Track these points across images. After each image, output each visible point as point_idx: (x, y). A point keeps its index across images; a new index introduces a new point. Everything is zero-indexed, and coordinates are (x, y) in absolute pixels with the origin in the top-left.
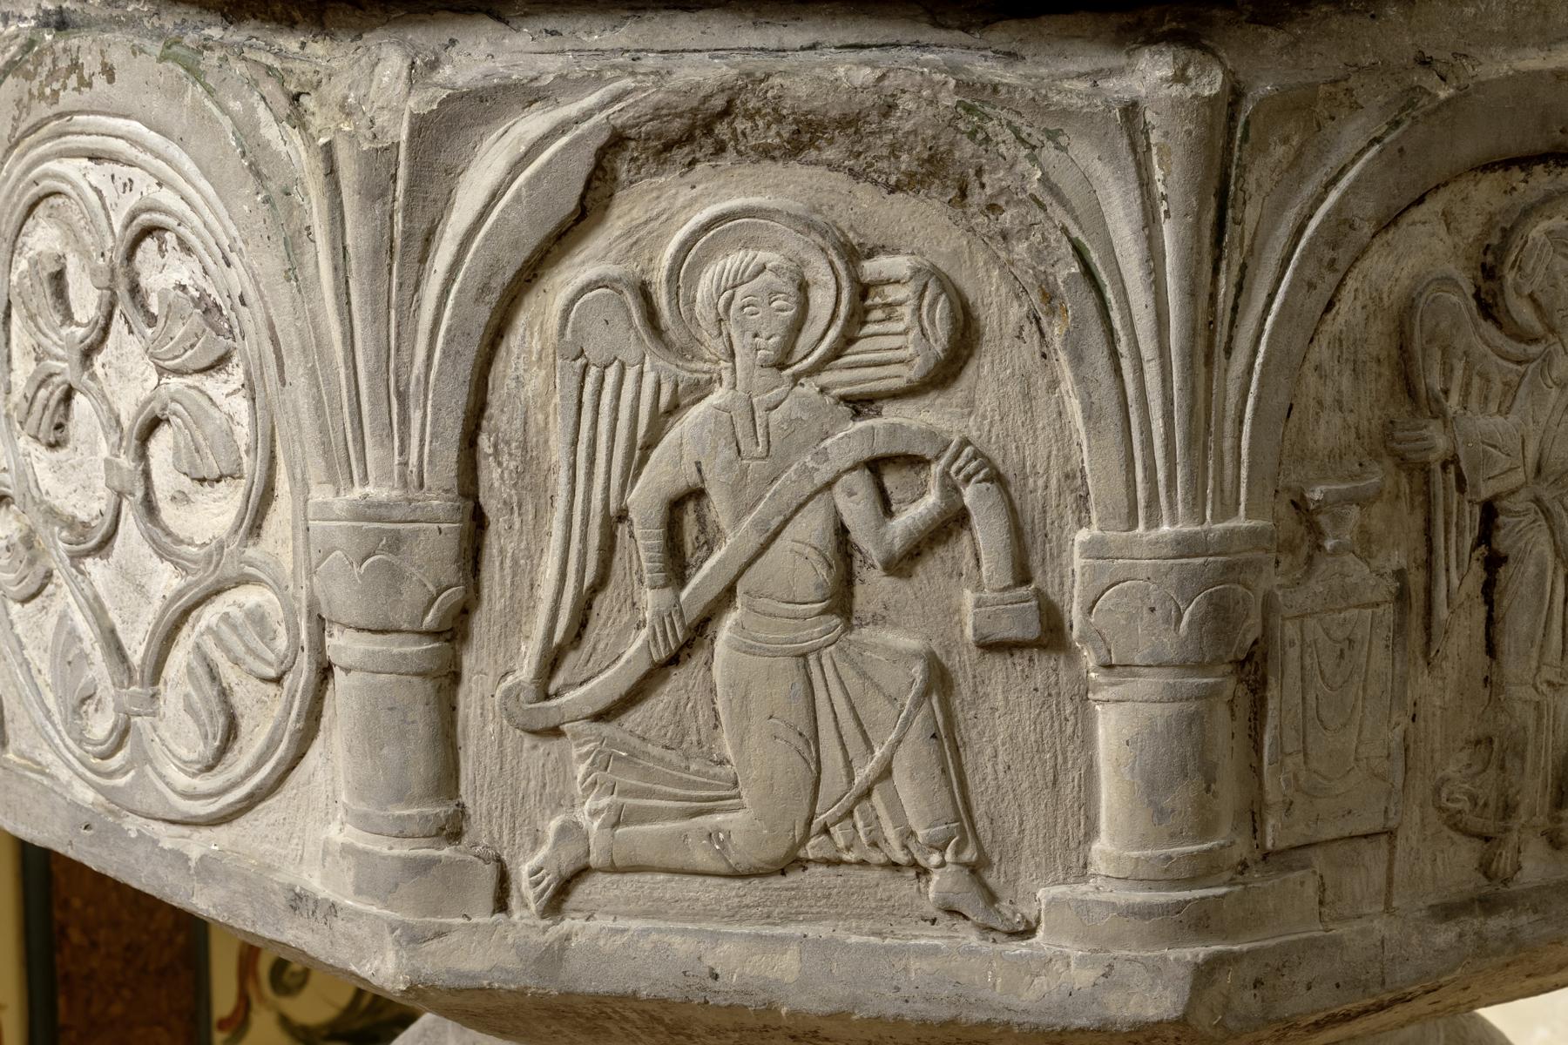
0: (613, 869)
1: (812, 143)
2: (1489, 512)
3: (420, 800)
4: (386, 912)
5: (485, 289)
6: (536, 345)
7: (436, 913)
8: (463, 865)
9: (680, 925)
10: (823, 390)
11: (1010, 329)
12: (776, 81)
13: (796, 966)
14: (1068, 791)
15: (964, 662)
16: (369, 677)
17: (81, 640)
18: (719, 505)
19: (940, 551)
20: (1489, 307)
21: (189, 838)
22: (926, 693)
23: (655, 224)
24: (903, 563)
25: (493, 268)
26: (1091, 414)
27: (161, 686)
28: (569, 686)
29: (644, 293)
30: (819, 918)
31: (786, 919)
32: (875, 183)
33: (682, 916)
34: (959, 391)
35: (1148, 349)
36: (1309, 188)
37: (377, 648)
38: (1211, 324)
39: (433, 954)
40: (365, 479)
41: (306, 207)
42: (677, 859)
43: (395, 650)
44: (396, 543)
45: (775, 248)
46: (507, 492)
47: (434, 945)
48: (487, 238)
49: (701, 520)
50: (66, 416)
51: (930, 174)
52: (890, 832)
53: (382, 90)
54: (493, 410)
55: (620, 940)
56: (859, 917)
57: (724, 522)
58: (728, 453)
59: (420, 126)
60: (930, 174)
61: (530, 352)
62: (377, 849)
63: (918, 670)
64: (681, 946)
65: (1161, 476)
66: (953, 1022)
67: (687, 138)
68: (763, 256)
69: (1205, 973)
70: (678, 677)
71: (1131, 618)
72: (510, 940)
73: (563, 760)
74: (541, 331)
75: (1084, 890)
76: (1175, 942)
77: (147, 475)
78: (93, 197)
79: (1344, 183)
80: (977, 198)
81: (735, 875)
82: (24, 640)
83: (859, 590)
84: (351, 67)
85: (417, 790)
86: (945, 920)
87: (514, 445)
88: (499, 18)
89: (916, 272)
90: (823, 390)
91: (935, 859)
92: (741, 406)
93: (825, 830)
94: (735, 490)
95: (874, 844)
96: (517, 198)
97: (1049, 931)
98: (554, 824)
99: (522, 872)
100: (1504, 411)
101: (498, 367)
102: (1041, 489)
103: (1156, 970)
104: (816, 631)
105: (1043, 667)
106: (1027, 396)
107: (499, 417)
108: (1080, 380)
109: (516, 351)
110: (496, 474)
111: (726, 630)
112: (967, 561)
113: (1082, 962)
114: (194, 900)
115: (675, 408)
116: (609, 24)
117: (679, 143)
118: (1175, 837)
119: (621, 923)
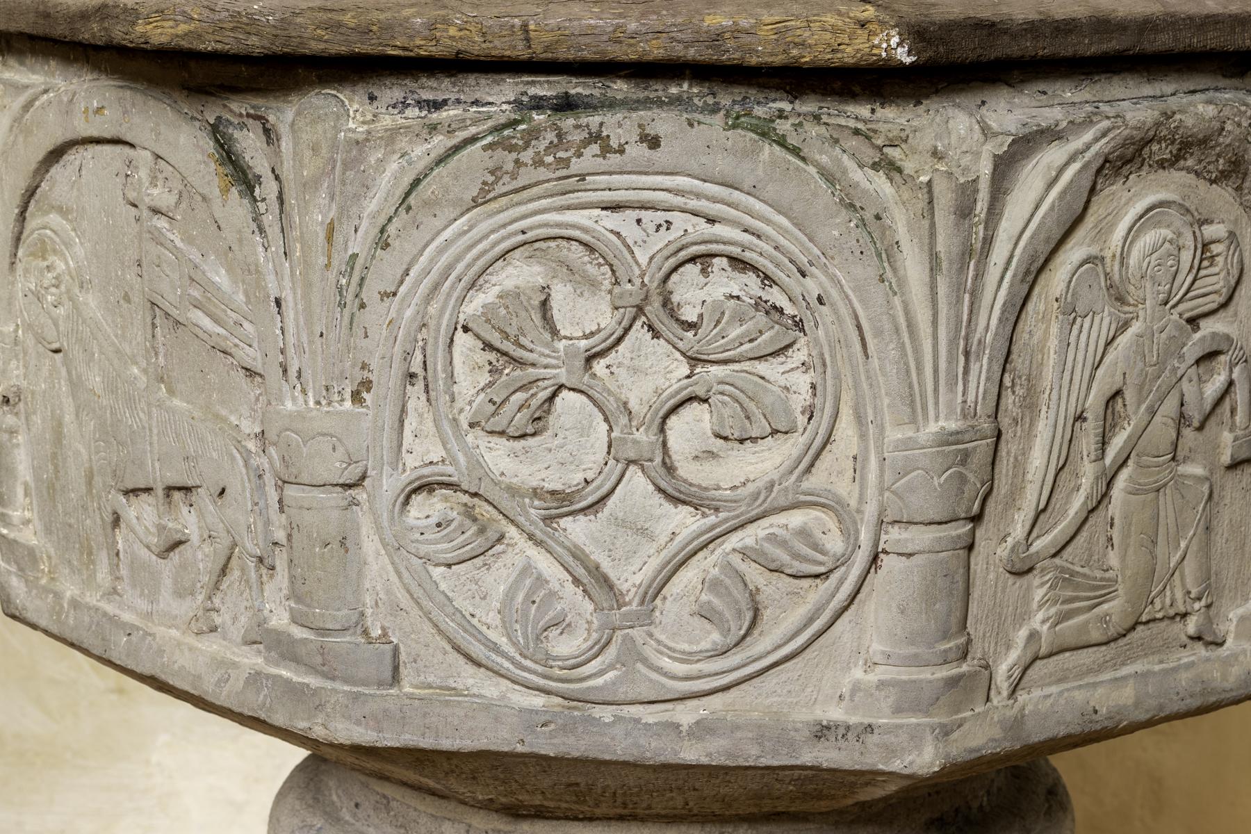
4: (927, 720)
6: (1042, 307)
9: (1076, 684)
10: (1181, 315)
12: (1178, 117)
16: (933, 556)
17: (547, 582)
18: (1129, 395)
21: (673, 710)
23: (1110, 218)
25: (1033, 259)
27: (658, 601)
28: (1038, 537)
32: (1205, 178)
37: (942, 534)
39: (956, 741)
41: (894, 227)
42: (1084, 639)
43: (954, 533)
46: (1016, 411)
48: (1032, 237)
50: (548, 412)
51: (1233, 171)
53: (962, 140)
55: (1050, 701)
56: (1153, 653)
60: (1233, 171)
61: (1038, 313)
62: (922, 676)
63: (1205, 488)
64: (1079, 696)
72: (996, 719)
73: (1029, 588)
74: (1046, 298)
77: (664, 444)
82: (450, 594)
84: (931, 124)
87: (1024, 378)
88: (1010, 85)
93: (1152, 603)
96: (1052, 208)
107: (1018, 361)
109: (1031, 313)
110: (1010, 401)
111: (1124, 475)
114: (682, 755)
116: (1073, 85)
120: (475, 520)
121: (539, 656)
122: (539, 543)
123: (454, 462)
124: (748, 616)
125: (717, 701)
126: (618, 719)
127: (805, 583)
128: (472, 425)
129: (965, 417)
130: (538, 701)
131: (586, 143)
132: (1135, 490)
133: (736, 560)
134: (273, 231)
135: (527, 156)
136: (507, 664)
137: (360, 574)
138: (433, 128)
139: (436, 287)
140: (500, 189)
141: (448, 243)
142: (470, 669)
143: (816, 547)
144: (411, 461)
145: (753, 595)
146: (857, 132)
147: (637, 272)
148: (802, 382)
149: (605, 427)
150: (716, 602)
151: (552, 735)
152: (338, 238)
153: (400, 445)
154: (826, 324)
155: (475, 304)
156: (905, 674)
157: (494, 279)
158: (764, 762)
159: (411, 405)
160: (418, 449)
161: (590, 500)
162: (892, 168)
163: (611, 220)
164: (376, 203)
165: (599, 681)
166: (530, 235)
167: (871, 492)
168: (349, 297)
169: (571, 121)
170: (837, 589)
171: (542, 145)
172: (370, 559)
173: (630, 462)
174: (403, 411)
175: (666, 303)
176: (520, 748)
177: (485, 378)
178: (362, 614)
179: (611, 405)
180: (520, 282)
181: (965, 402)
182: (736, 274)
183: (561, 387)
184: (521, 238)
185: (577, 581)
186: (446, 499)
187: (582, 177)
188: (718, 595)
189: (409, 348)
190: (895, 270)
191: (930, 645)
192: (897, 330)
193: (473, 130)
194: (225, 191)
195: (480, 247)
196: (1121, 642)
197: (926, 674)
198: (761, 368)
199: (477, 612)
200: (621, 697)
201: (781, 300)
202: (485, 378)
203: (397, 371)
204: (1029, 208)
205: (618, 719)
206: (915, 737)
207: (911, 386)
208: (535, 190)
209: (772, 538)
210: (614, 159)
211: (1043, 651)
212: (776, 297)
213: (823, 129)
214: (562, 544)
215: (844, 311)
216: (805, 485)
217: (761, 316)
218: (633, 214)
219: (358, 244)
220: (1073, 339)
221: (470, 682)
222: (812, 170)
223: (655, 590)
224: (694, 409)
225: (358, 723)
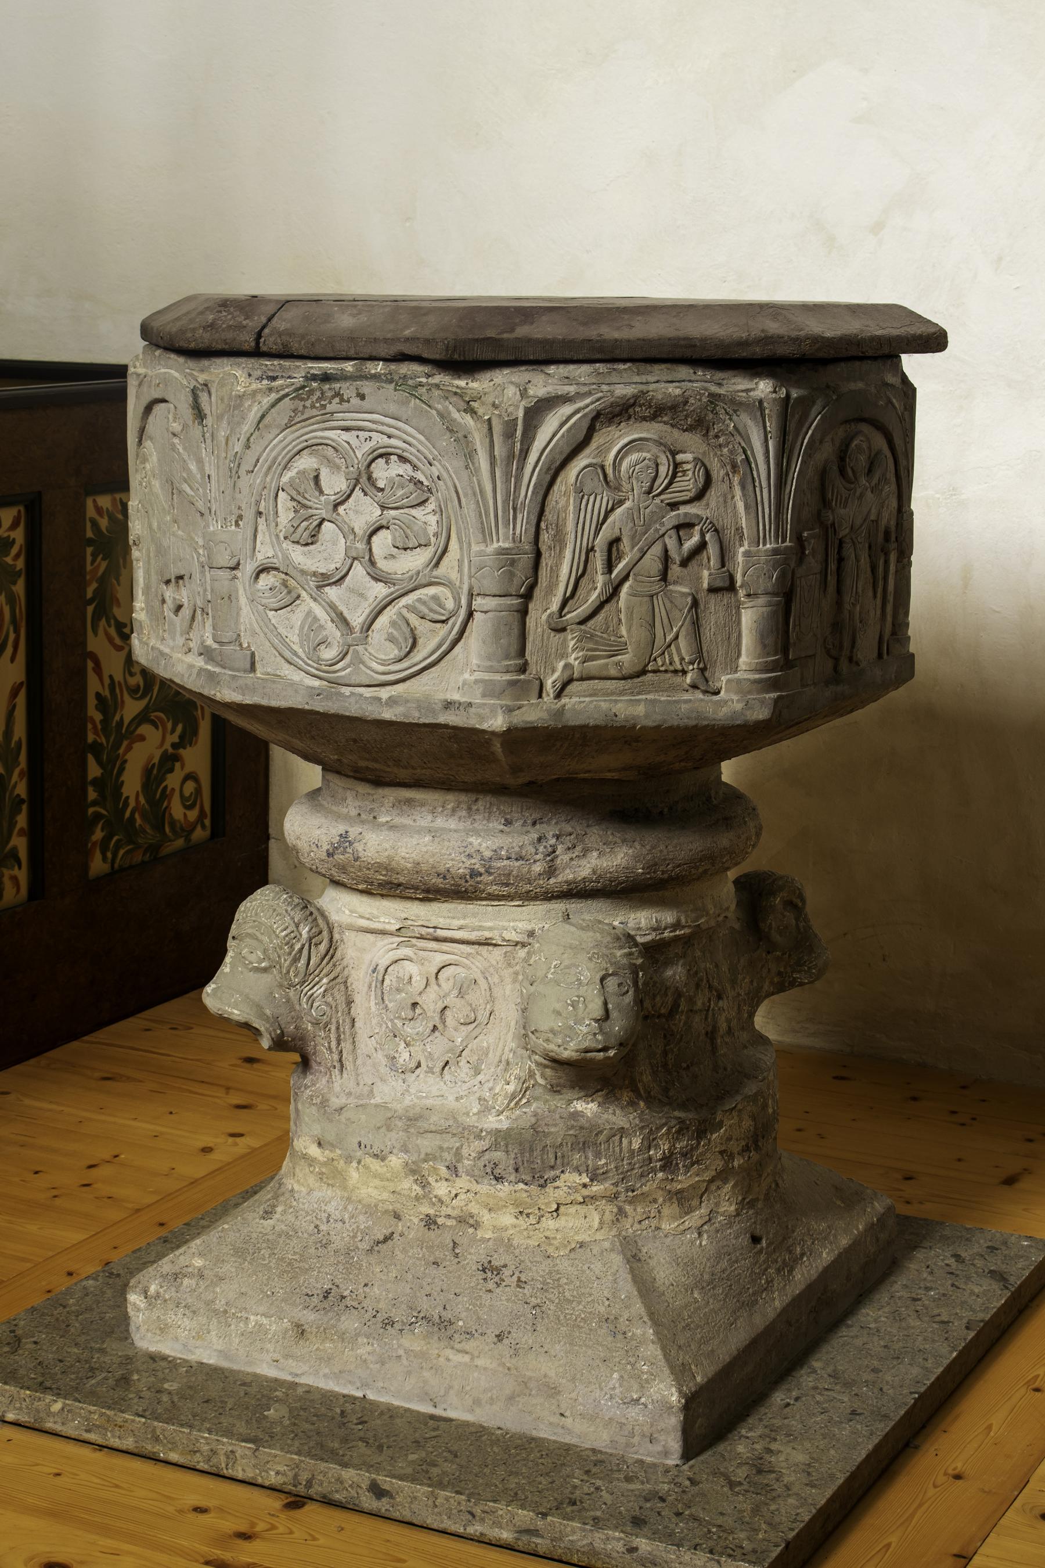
0: (582, 679)
1: (659, 415)
2: (841, 543)
3: (514, 658)
5: (549, 469)
6: (563, 489)
7: (518, 700)
8: (529, 681)
10: (662, 501)
11: (720, 478)
13: (643, 710)
14: (733, 641)
15: (702, 596)
16: (498, 614)
18: (626, 542)
19: (697, 557)
20: (842, 472)
22: (691, 608)
24: (684, 563)
25: (552, 462)
26: (747, 507)
27: (370, 632)
28: (569, 612)
29: (603, 467)
30: (649, 692)
31: (639, 693)
33: (604, 695)
34: (704, 502)
35: (764, 484)
36: (804, 429)
38: (781, 475)
40: (498, 541)
42: (604, 673)
44: (513, 563)
45: (648, 452)
47: (517, 712)
48: (551, 450)
49: (618, 550)
50: (318, 532)
52: (676, 659)
53: (509, 399)
54: (547, 513)
55: (583, 705)
57: (627, 549)
58: (631, 525)
59: (528, 411)
63: (689, 600)
64: (604, 706)
65: (767, 528)
67: (620, 414)
68: (644, 454)
69: (776, 701)
70: (607, 607)
71: (758, 577)
73: (565, 640)
75: (738, 675)
76: (768, 692)
77: (370, 550)
78: (346, 445)
79: (813, 427)
80: (711, 433)
81: (624, 678)
83: (670, 572)
85: (513, 654)
86: (691, 690)
89: (695, 459)
90: (662, 501)
91: (691, 667)
92: (636, 507)
93: (655, 660)
94: (633, 537)
95: (671, 664)
96: (563, 436)
97: (726, 691)
98: (561, 664)
99: (549, 683)
100: (845, 507)
101: (550, 497)
102: (729, 533)
103: (762, 702)
104: (656, 588)
105: (726, 598)
106: (725, 502)
107: (549, 515)
108: (744, 495)
110: (546, 536)
111: (625, 588)
112: (705, 560)
113: (738, 701)
115: (613, 509)
117: (617, 416)
118: (768, 655)
119: (582, 699)
120: (286, 587)
121: (315, 658)
122: (315, 600)
123: (277, 558)
124: (410, 641)
125: (400, 688)
126: (352, 694)
127: (438, 625)
128: (286, 538)
130: (317, 683)
131: (333, 397)
132: (633, 594)
133: (404, 611)
134: (209, 441)
135: (308, 403)
136: (301, 662)
137: (238, 614)
138: (270, 390)
139: (270, 468)
140: (297, 419)
141: (275, 446)
142: (287, 666)
143: (440, 606)
144: (260, 557)
145: (412, 631)
146: (456, 393)
147: (356, 461)
148: (433, 519)
149: (343, 540)
150: (395, 633)
152: (230, 443)
153: (254, 548)
154: (443, 490)
155: (285, 479)
156: (487, 676)
157: (295, 465)
158: (422, 721)
159: (260, 528)
160: (263, 550)
161: (337, 578)
162: (473, 412)
163: (345, 436)
164: (246, 428)
165: (343, 673)
166: (310, 443)
167: (466, 578)
168: (234, 472)
169: (327, 386)
170: (452, 629)
171: (315, 398)
172: (243, 607)
173: (354, 559)
174: (256, 530)
175: (370, 478)
176: (307, 707)
177: (292, 515)
178: (239, 635)
179: (346, 529)
180: (306, 466)
181: (514, 534)
182: (401, 464)
183: (324, 520)
184: (305, 444)
185: (332, 621)
186: (275, 576)
187: (332, 414)
188: (396, 629)
189: (258, 498)
190: (473, 463)
191: (499, 662)
192: (475, 494)
193: (287, 390)
194: (194, 422)
195: (288, 448)
196: (636, 680)
197: (497, 677)
198: (413, 512)
199: (289, 635)
200: (353, 682)
201: (422, 478)
202: (292, 515)
203: (253, 510)
204: (549, 436)
205: (352, 694)
206: (493, 710)
207: (482, 523)
208: (312, 420)
209: (419, 600)
210: (345, 405)
211: (576, 675)
212: (420, 476)
213: (440, 392)
214: (324, 600)
215: (450, 484)
216: (435, 573)
217: (411, 486)
218: (355, 433)
219: (238, 447)
220: (583, 507)
221: (287, 672)
222: (434, 412)
223: (368, 626)
224: (383, 533)
225: (234, 691)
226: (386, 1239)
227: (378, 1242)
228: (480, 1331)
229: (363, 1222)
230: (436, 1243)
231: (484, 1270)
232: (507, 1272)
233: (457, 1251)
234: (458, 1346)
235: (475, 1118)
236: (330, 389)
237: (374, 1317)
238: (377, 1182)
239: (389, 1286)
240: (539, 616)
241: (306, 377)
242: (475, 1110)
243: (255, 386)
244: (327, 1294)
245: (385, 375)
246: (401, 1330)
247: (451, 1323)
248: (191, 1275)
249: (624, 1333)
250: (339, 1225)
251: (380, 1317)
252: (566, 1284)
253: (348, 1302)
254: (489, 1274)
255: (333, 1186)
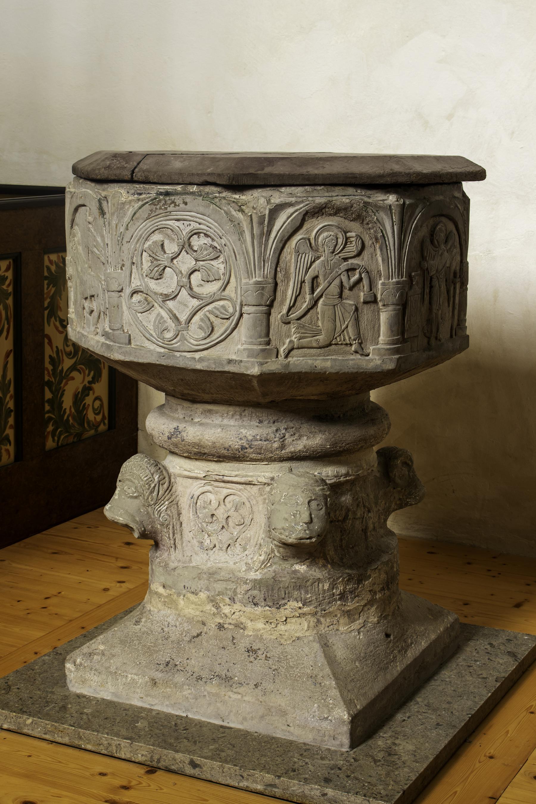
0: (298, 348)
1: (338, 213)
2: (431, 278)
3: (264, 337)
5: (282, 240)
6: (289, 251)
7: (266, 359)
8: (271, 349)
10: (339, 257)
11: (369, 245)
13: (330, 364)
14: (376, 328)
15: (360, 306)
16: (255, 315)
18: (321, 278)
19: (358, 286)
20: (432, 242)
22: (354, 312)
24: (351, 289)
25: (283, 237)
26: (383, 260)
27: (190, 324)
28: (292, 314)
29: (309, 240)
30: (333, 355)
31: (328, 356)
33: (310, 356)
34: (361, 257)
35: (392, 248)
36: (413, 220)
38: (401, 243)
40: (256, 277)
42: (310, 345)
45: (333, 232)
47: (265, 365)
48: (283, 231)
49: (317, 282)
50: (163, 273)
52: (347, 338)
53: (261, 205)
54: (280, 263)
55: (299, 362)
57: (322, 282)
58: (324, 269)
59: (271, 211)
63: (354, 307)
64: (310, 362)
65: (394, 271)
66: (357, 372)
67: (318, 212)
68: (331, 233)
70: (311, 311)
71: (389, 296)
73: (290, 328)
75: (379, 346)
76: (394, 355)
77: (190, 282)
78: (177, 228)
79: (417, 219)
80: (365, 222)
81: (320, 348)
83: (343, 293)
85: (263, 335)
86: (354, 354)
89: (356, 235)
90: (339, 257)
91: (354, 342)
92: (326, 260)
93: (336, 338)
94: (325, 275)
95: (344, 340)
96: (289, 223)
99: (281, 350)
100: (433, 260)
101: (282, 255)
102: (374, 273)
103: (391, 360)
104: (336, 301)
105: (373, 306)
106: (372, 257)
107: (282, 264)
108: (382, 254)
110: (280, 275)
111: (321, 302)
112: (362, 287)
113: (379, 359)
115: (314, 261)
117: (317, 213)
118: (394, 336)
119: (299, 359)
120: (147, 301)
121: (162, 338)
122: (162, 308)
123: (142, 286)
124: (211, 329)
125: (205, 353)
126: (181, 356)
127: (225, 321)
128: (146, 276)
129: (264, 278)
130: (162, 350)
131: (171, 204)
132: (324, 305)
133: (207, 314)
134: (107, 226)
135: (158, 207)
136: (154, 340)
137: (122, 315)
138: (139, 200)
139: (138, 240)
140: (152, 215)
141: (141, 229)
142: (147, 341)
143: (226, 311)
144: (133, 285)
145: (211, 323)
146: (234, 202)
147: (183, 237)
150: (203, 324)
151: (165, 359)
152: (118, 227)
153: (131, 281)
154: (227, 251)
156: (250, 347)
157: (151, 238)
158: (217, 369)
159: (133, 271)
160: (135, 282)
161: (173, 296)
162: (242, 211)
163: (177, 223)
164: (126, 219)
165: (176, 345)
166: (159, 227)
167: (239, 296)
168: (120, 242)
169: (168, 198)
170: (232, 322)
171: (161, 204)
172: (125, 311)
173: (182, 286)
174: (131, 272)
175: (190, 245)
176: (157, 363)
177: (150, 264)
178: (123, 326)
179: (177, 271)
180: (157, 239)
181: (264, 274)
182: (206, 238)
183: (166, 266)
184: (157, 228)
185: (171, 318)
186: (141, 296)
187: (170, 212)
188: (203, 323)
189: (132, 256)
190: (243, 238)
191: (256, 339)
192: (243, 253)
193: (147, 200)
194: (99, 217)
195: (148, 230)
196: (326, 349)
197: (255, 347)
198: (212, 262)
199: (148, 326)
200: (181, 350)
202: (150, 264)
203: (130, 262)
204: (282, 223)
205: (181, 356)
206: (253, 364)
207: (247, 268)
208: (160, 216)
209: (215, 308)
210: (177, 208)
211: (295, 346)
212: (215, 244)
213: (226, 201)
214: (166, 308)
215: (231, 248)
216: (223, 294)
217: (211, 249)
218: (182, 222)
219: (122, 229)
220: (299, 260)
221: (147, 345)
222: (223, 211)
223: (189, 321)
224: (196, 273)
225: (120, 354)
226: (198, 635)
227: (194, 637)
228: (246, 683)
229: (186, 626)
230: (224, 637)
231: (248, 651)
232: (260, 652)
233: (234, 641)
234: (235, 690)
235: (243, 573)
236: (169, 199)
237: (192, 675)
238: (193, 606)
239: (199, 659)
240: (276, 316)
241: (157, 193)
242: (244, 569)
243: (131, 198)
244: (168, 664)
245: (198, 192)
246: (206, 682)
247: (231, 678)
248: (98, 654)
249: (320, 684)
250: (174, 628)
251: (195, 675)
252: (290, 658)
253: (179, 668)
254: (251, 653)
255: (171, 608)
